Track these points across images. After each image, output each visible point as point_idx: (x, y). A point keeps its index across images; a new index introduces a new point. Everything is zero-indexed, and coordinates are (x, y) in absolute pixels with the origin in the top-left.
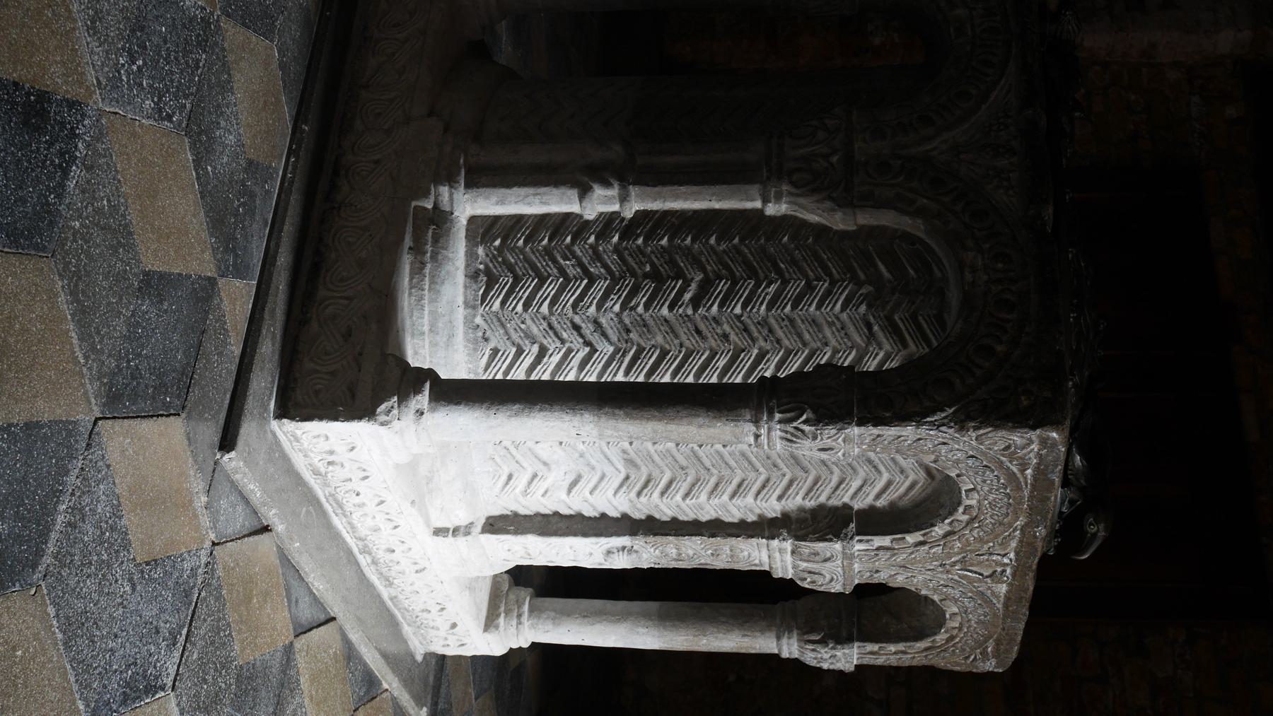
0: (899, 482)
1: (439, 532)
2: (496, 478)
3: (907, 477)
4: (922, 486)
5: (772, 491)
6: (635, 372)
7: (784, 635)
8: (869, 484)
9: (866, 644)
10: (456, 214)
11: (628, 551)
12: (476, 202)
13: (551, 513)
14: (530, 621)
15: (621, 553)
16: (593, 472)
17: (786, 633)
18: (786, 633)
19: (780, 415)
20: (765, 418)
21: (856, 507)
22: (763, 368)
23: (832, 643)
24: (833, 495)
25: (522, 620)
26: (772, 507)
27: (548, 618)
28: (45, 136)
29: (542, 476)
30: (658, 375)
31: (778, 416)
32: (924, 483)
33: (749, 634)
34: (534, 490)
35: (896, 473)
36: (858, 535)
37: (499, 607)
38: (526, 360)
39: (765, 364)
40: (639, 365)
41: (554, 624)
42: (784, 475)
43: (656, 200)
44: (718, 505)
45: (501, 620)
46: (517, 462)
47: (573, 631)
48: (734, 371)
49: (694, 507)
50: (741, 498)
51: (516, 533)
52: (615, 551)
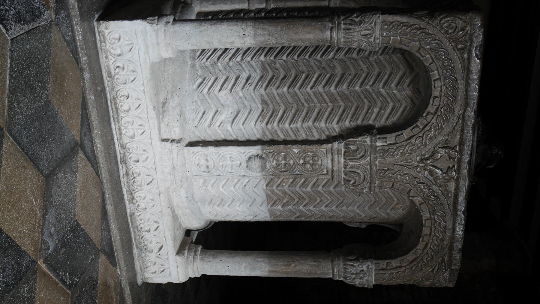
0: (398, 106)
1: (163, 140)
2: (197, 112)
3: (401, 104)
4: (409, 109)
5: (334, 117)
6: (270, 54)
7: (335, 259)
8: (383, 109)
9: (379, 261)
10: (193, 5)
11: (260, 157)
12: (202, 3)
13: (222, 140)
14: (201, 256)
15: (256, 158)
16: (246, 108)
17: (337, 258)
18: (337, 258)
19: (343, 17)
20: (336, 18)
21: (377, 126)
22: (330, 51)
23: (361, 259)
24: (365, 118)
25: (197, 253)
26: (335, 128)
27: (210, 255)
28: (16, 110)
29: (220, 111)
30: (281, 55)
31: (342, 18)
32: (410, 107)
33: (317, 260)
34: (215, 121)
35: (396, 101)
36: (379, 134)
37: (185, 247)
38: (219, 52)
39: (331, 49)
40: (272, 51)
41: (213, 257)
42: (340, 106)
43: (282, 2)
44: (307, 127)
45: (186, 252)
46: (208, 103)
47: (223, 261)
48: (317, 52)
49: (295, 130)
50: (319, 122)
51: (203, 146)
52: (253, 157)
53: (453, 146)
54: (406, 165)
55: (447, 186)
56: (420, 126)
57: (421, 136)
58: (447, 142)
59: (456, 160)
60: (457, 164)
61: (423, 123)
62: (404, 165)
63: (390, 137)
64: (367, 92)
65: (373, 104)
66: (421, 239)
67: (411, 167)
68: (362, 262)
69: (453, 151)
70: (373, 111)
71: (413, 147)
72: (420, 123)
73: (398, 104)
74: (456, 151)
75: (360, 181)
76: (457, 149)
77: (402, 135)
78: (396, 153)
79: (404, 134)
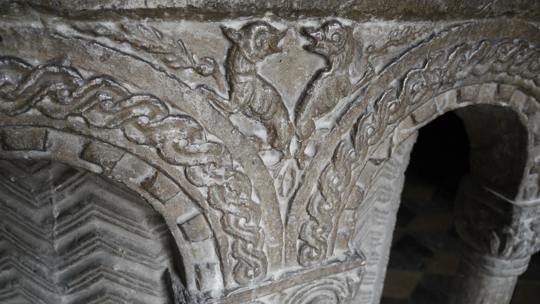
9: (521, 189)
23: (507, 230)
53: (226, 44)
54: (289, 191)
55: (374, 47)
56: (145, 176)
57: (185, 172)
58: (209, 69)
59: (280, 26)
60: (296, 19)
61: (133, 166)
62: (291, 195)
63: (195, 256)
64: (70, 284)
65: (101, 273)
66: (504, 104)
67: (299, 173)
68: (516, 230)
69: (246, 45)
70: (122, 274)
71: (227, 190)
72: (134, 177)
73: (92, 208)
74: (247, 28)
75: (326, 297)
76: (235, 25)
77: (185, 226)
78: (247, 235)
79: (181, 219)
